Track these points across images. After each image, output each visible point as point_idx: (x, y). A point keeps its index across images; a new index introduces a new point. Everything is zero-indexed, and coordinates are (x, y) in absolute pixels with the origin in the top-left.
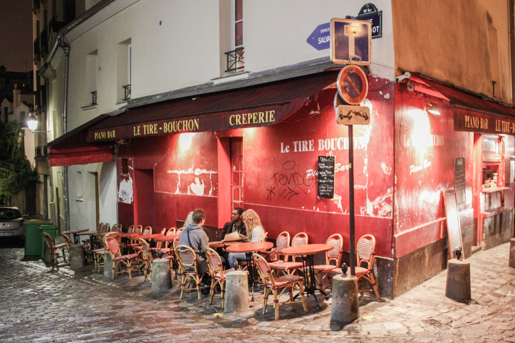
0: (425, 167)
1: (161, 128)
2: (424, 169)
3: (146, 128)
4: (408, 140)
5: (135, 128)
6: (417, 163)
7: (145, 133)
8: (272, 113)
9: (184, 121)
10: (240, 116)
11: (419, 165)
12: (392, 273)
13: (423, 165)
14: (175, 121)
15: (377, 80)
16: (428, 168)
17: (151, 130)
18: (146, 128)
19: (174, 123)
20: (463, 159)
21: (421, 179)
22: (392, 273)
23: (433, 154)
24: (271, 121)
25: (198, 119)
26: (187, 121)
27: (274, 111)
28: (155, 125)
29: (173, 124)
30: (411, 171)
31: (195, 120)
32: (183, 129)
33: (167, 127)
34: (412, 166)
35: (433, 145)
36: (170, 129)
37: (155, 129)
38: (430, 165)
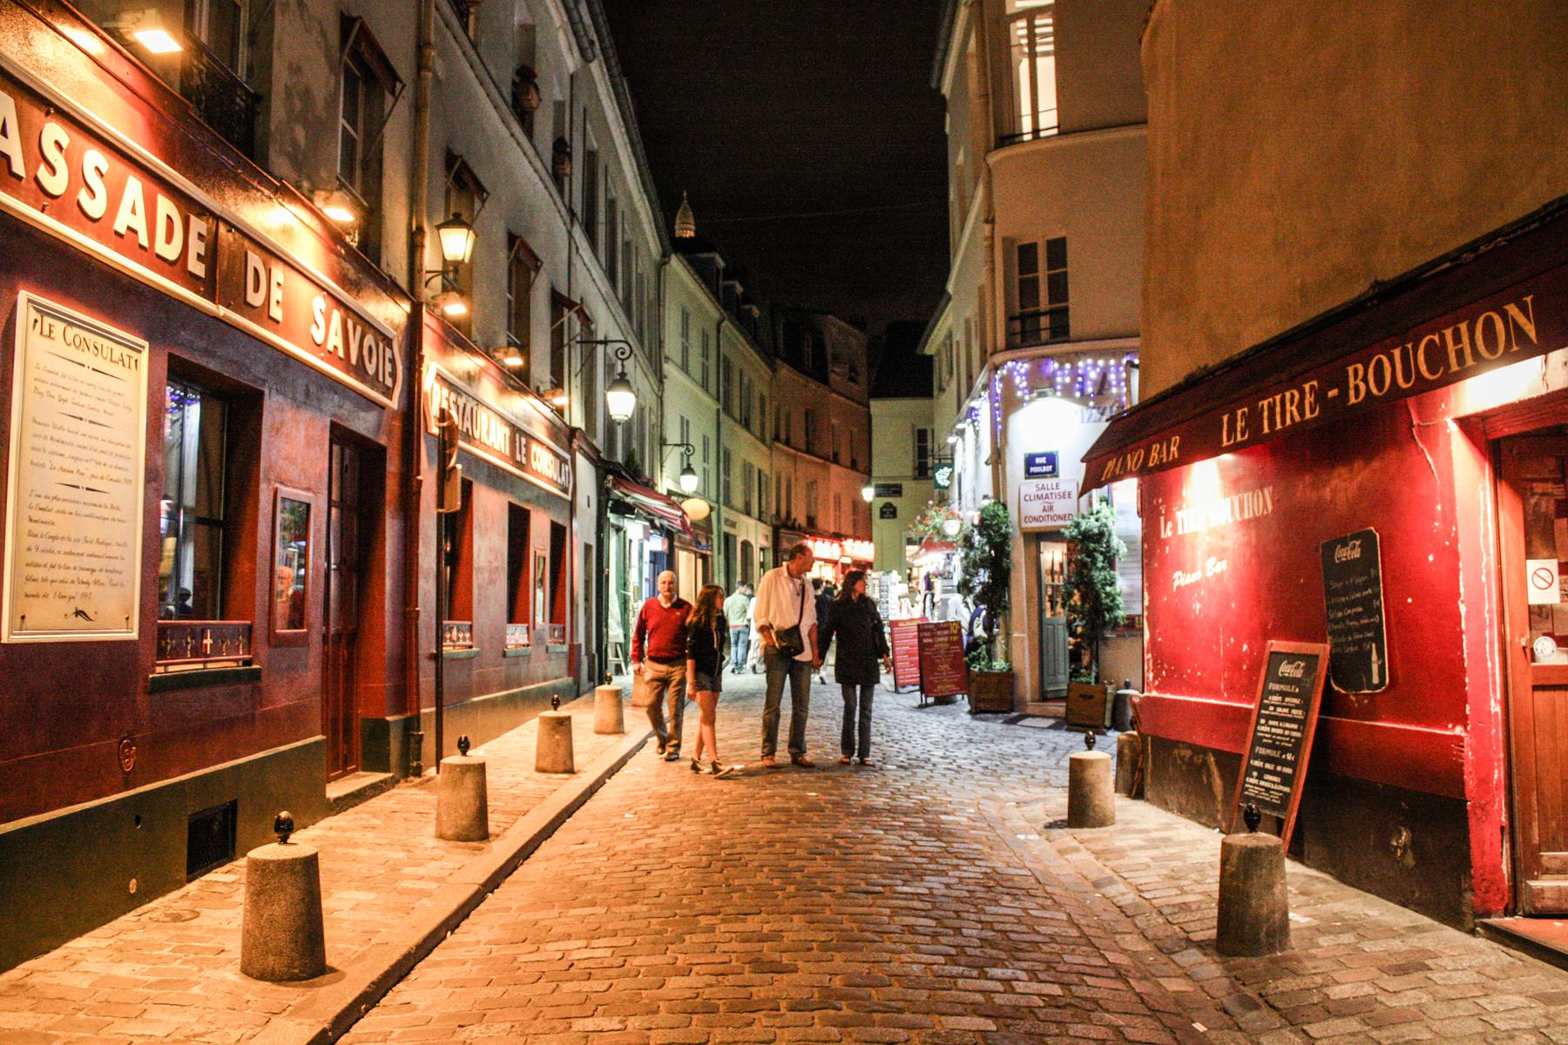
0: (1209, 574)
1: (1333, 393)
2: (1207, 578)
3: (1272, 408)
4: (1170, 524)
5: (1225, 418)
6: (1188, 567)
7: (1266, 430)
8: (1312, 387)
9: (1448, 333)
10: (1296, 393)
11: (1193, 571)
12: (286, 458)
13: (1204, 570)
14: (1402, 344)
15: (133, 886)
16: (1219, 577)
17: (1292, 409)
18: (1272, 408)
19: (1397, 353)
20: (1368, 540)
21: (1200, 600)
22: (286, 458)
23: (1234, 540)
24: (1308, 415)
25: (1528, 299)
26: (1463, 327)
27: (1315, 383)
28: (1307, 387)
29: (1392, 366)
30: (1176, 584)
31: (1512, 310)
32: (1448, 366)
33: (1365, 380)
34: (1177, 574)
35: (1231, 521)
36: (1380, 382)
37: (1309, 399)
38: (1225, 568)
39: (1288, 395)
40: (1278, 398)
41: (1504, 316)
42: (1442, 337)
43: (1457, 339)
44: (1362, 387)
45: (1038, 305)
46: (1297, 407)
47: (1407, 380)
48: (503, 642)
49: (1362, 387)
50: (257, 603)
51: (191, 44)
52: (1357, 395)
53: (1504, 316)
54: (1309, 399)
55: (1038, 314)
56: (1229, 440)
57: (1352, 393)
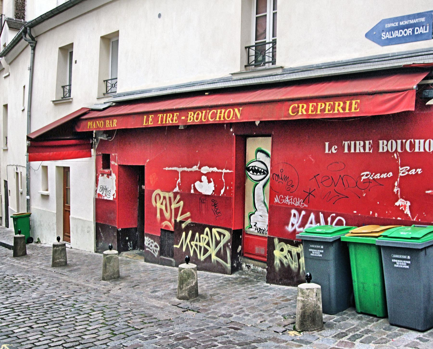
1: (183, 118)
3: (162, 118)
17: (169, 119)
18: (162, 118)
28: (175, 114)
33: (193, 117)
39: (168, 115)
40: (219, 111)
41: (234, 111)
42: (217, 111)
43: (221, 113)
44: (192, 118)
45: (265, 38)
46: (305, 110)
47: (205, 119)
48: (322, 318)
49: (192, 118)
50: (116, 242)
51: (350, 308)
52: (190, 120)
53: (234, 111)
54: (175, 118)
55: (265, 43)
56: (146, 123)
57: (189, 119)
